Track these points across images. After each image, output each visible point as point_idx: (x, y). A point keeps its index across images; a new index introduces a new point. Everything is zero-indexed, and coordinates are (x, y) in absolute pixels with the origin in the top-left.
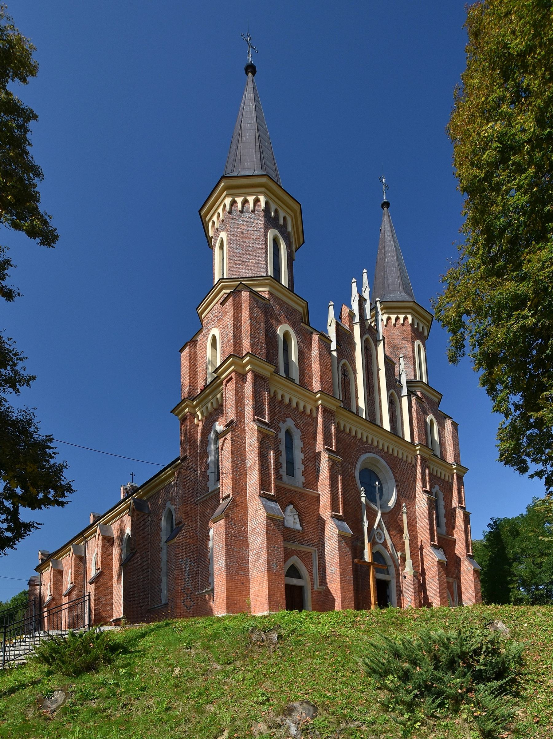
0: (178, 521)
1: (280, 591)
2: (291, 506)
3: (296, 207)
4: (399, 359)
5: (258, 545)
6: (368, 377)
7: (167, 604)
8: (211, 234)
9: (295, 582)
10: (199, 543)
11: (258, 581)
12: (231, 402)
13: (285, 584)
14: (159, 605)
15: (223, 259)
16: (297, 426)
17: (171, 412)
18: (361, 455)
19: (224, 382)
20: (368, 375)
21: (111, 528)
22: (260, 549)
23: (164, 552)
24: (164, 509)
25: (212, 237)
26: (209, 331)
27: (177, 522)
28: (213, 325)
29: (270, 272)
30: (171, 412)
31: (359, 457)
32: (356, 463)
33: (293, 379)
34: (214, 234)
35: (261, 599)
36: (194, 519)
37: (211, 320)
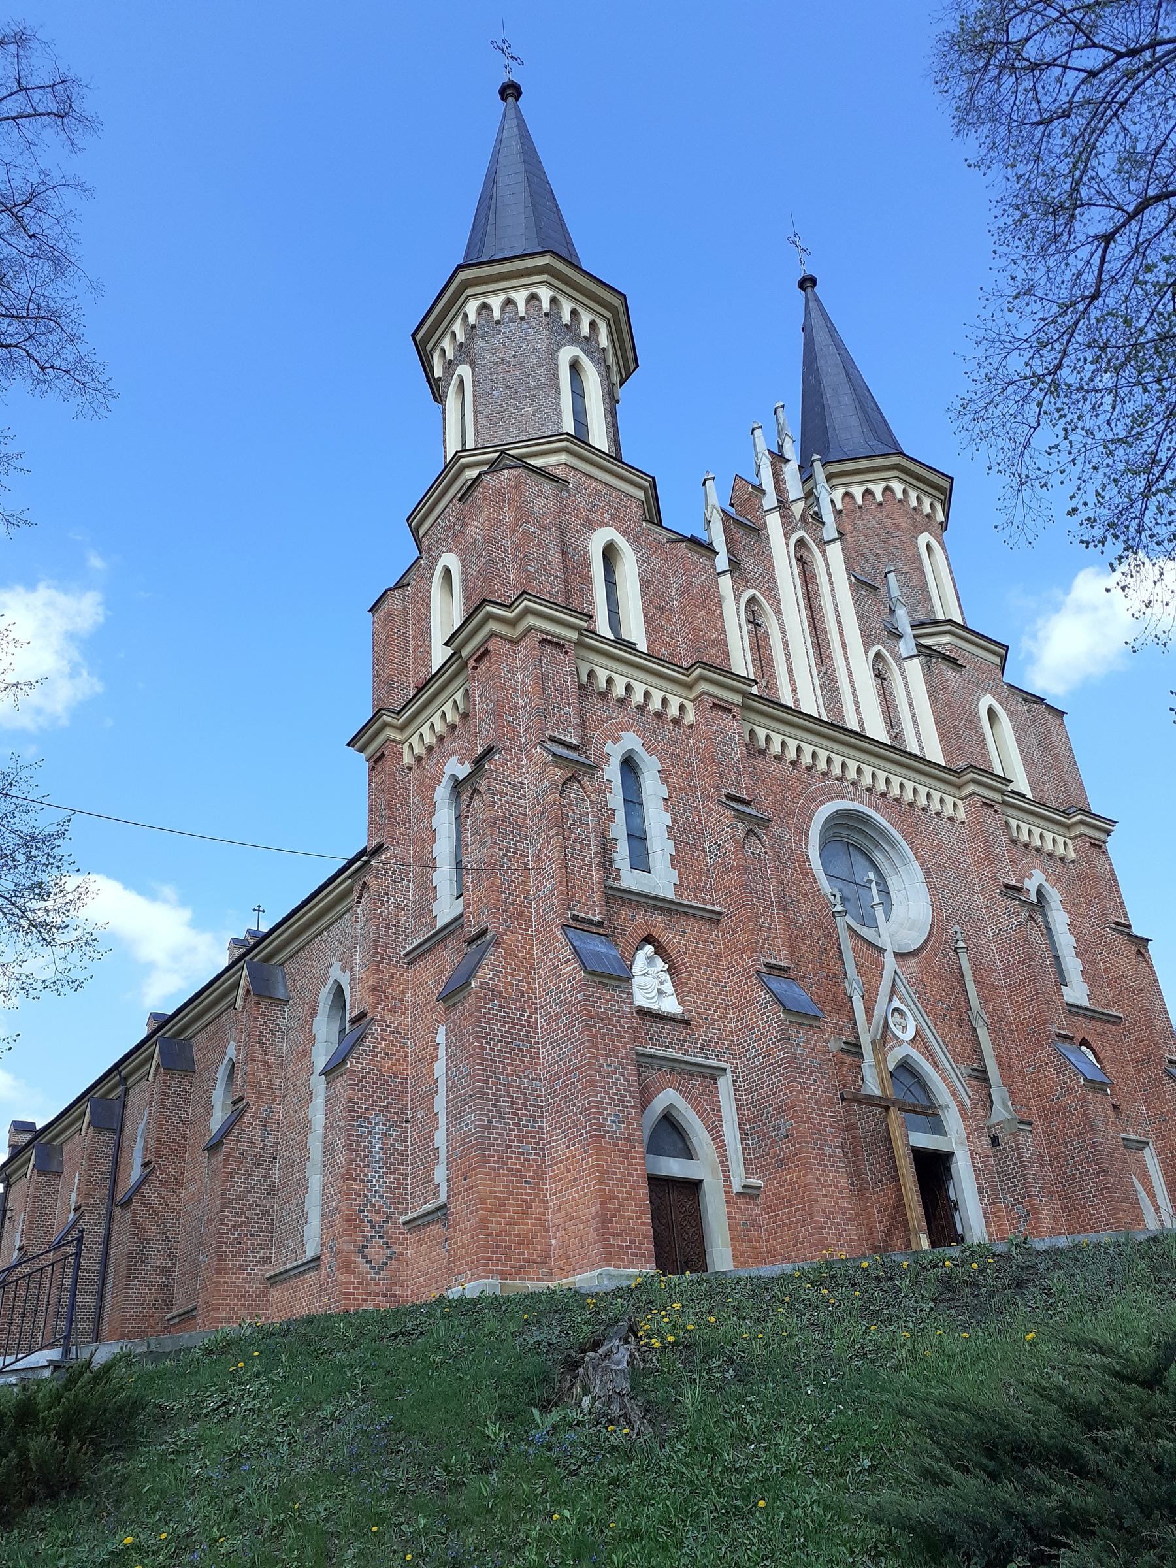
0: (356, 1012)
1: (633, 1199)
2: (649, 949)
3: (615, 301)
4: (886, 576)
5: (565, 1063)
6: (814, 624)
7: (317, 1259)
8: (438, 372)
9: (674, 1167)
10: (411, 1071)
11: (568, 1170)
12: (488, 705)
13: (649, 1178)
14: (299, 1262)
15: (463, 416)
16: (648, 748)
17: (348, 745)
18: (818, 807)
19: (471, 663)
20: (813, 619)
21: (191, 1046)
22: (571, 1072)
23: (319, 1102)
24: (324, 983)
25: (440, 379)
26: (434, 561)
27: (353, 1015)
28: (443, 546)
29: (569, 426)
30: (348, 745)
31: (813, 813)
32: (809, 827)
33: (631, 643)
34: (444, 373)
35: (582, 1226)
36: (399, 1003)
37: (440, 539)
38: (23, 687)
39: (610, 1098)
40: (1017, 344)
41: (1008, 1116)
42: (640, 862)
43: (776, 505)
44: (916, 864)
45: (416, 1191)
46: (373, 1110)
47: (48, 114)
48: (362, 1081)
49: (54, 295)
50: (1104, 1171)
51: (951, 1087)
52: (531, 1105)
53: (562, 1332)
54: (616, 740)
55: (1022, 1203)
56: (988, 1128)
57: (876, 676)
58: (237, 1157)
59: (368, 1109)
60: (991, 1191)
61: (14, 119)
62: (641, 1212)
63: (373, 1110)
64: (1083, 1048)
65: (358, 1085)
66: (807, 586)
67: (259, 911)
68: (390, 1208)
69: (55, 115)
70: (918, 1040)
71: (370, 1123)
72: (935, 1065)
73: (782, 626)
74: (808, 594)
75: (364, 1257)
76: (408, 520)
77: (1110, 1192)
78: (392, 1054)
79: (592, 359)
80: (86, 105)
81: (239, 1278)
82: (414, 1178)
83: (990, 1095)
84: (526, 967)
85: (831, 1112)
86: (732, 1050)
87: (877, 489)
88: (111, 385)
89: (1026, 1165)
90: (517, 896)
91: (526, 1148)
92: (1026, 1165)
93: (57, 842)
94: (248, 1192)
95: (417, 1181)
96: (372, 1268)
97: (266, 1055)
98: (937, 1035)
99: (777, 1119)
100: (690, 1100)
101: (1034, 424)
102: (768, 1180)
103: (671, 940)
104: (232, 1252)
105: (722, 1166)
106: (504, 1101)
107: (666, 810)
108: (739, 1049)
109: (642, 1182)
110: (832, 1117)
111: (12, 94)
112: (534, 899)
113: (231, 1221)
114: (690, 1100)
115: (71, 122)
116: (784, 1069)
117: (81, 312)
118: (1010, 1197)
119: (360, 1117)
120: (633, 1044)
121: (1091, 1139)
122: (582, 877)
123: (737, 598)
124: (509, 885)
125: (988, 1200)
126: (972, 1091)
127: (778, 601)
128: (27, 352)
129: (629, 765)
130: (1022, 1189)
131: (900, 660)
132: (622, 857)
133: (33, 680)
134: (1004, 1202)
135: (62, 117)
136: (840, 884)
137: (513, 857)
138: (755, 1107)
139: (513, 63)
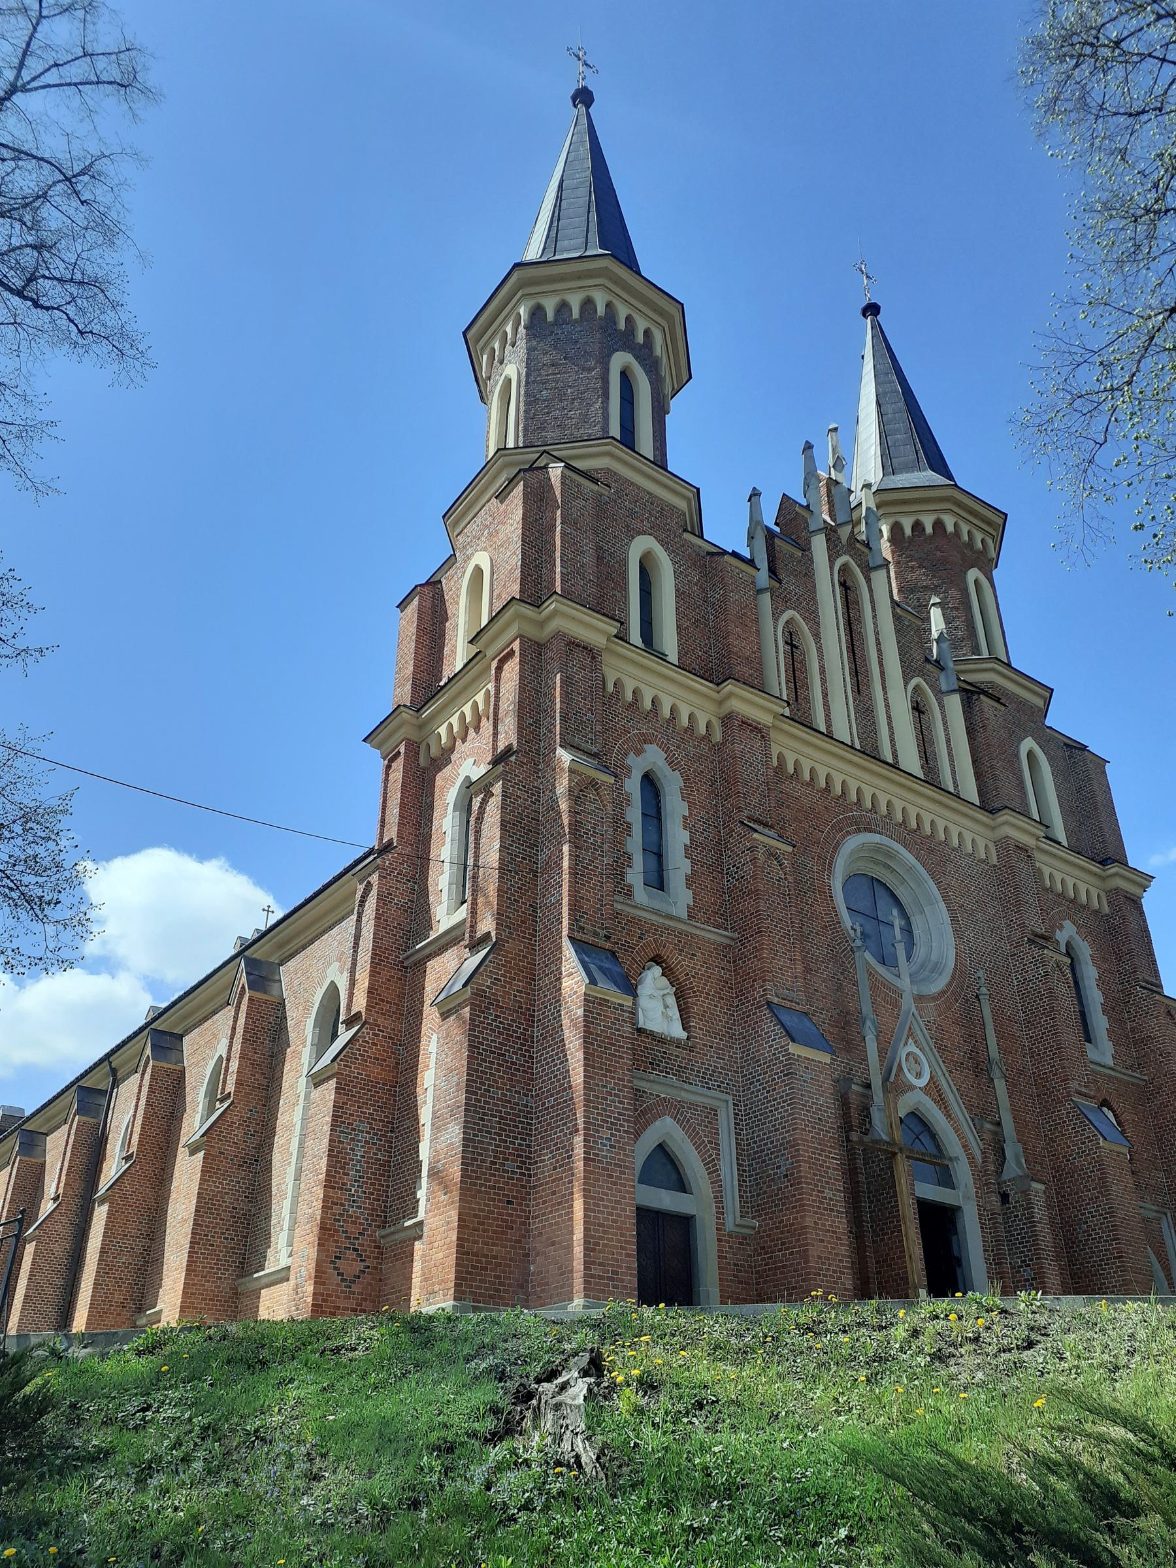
9: (666, 1200)
17: (364, 740)
30: (364, 740)
38: (33, 652)
39: (602, 1121)
40: (1087, 357)
41: (1020, 1173)
42: (658, 881)
43: (823, 526)
44: (943, 905)
45: (396, 1205)
46: (357, 1116)
47: (111, 83)
48: (349, 1086)
49: (99, 261)
50: (1118, 1239)
51: (963, 1138)
52: (520, 1122)
53: (519, 1358)
54: (639, 752)
55: (1029, 1265)
56: (998, 1184)
57: (913, 708)
58: (217, 1156)
59: (353, 1115)
60: (997, 1250)
61: (75, 85)
62: (626, 1242)
63: (357, 1116)
64: (1105, 1109)
65: (344, 1089)
66: (848, 612)
67: (268, 911)
68: (367, 1220)
69: (119, 84)
70: (933, 1090)
71: (354, 1130)
72: (948, 1116)
73: (820, 650)
74: (849, 620)
75: (335, 1268)
76: (444, 517)
77: (1123, 1262)
78: (382, 1060)
79: (643, 366)
80: (151, 77)
81: (209, 1281)
82: (395, 1190)
83: (1003, 1149)
84: (527, 978)
85: (835, 1154)
86: (736, 1081)
88: (149, 354)
89: (1035, 1226)
90: (523, 903)
91: (511, 1166)
92: (1035, 1226)
93: (59, 817)
94: (226, 1193)
95: (397, 1194)
96: (343, 1280)
97: (255, 1053)
98: (952, 1083)
99: (777, 1157)
100: (688, 1130)
101: (1101, 439)
102: (763, 1220)
103: (680, 962)
104: (204, 1254)
105: (716, 1202)
106: (492, 1115)
107: (685, 828)
108: (743, 1082)
109: (631, 1212)
110: (835, 1159)
111: (77, 59)
112: (541, 907)
113: (205, 1221)
114: (688, 1130)
115: (133, 93)
116: (788, 1105)
117: (126, 279)
118: (1018, 1258)
119: (344, 1123)
120: (631, 1066)
121: (1106, 1204)
122: (591, 888)
123: (776, 618)
124: (515, 891)
125: (994, 1260)
126: (984, 1144)
127: (818, 623)
128: (67, 315)
129: (649, 780)
130: (1031, 1251)
131: (940, 694)
132: (635, 876)
133: (44, 646)
134: (1010, 1263)
135: (125, 87)
136: (860, 919)
137: (522, 863)
138: (755, 1142)
139: (588, 72)
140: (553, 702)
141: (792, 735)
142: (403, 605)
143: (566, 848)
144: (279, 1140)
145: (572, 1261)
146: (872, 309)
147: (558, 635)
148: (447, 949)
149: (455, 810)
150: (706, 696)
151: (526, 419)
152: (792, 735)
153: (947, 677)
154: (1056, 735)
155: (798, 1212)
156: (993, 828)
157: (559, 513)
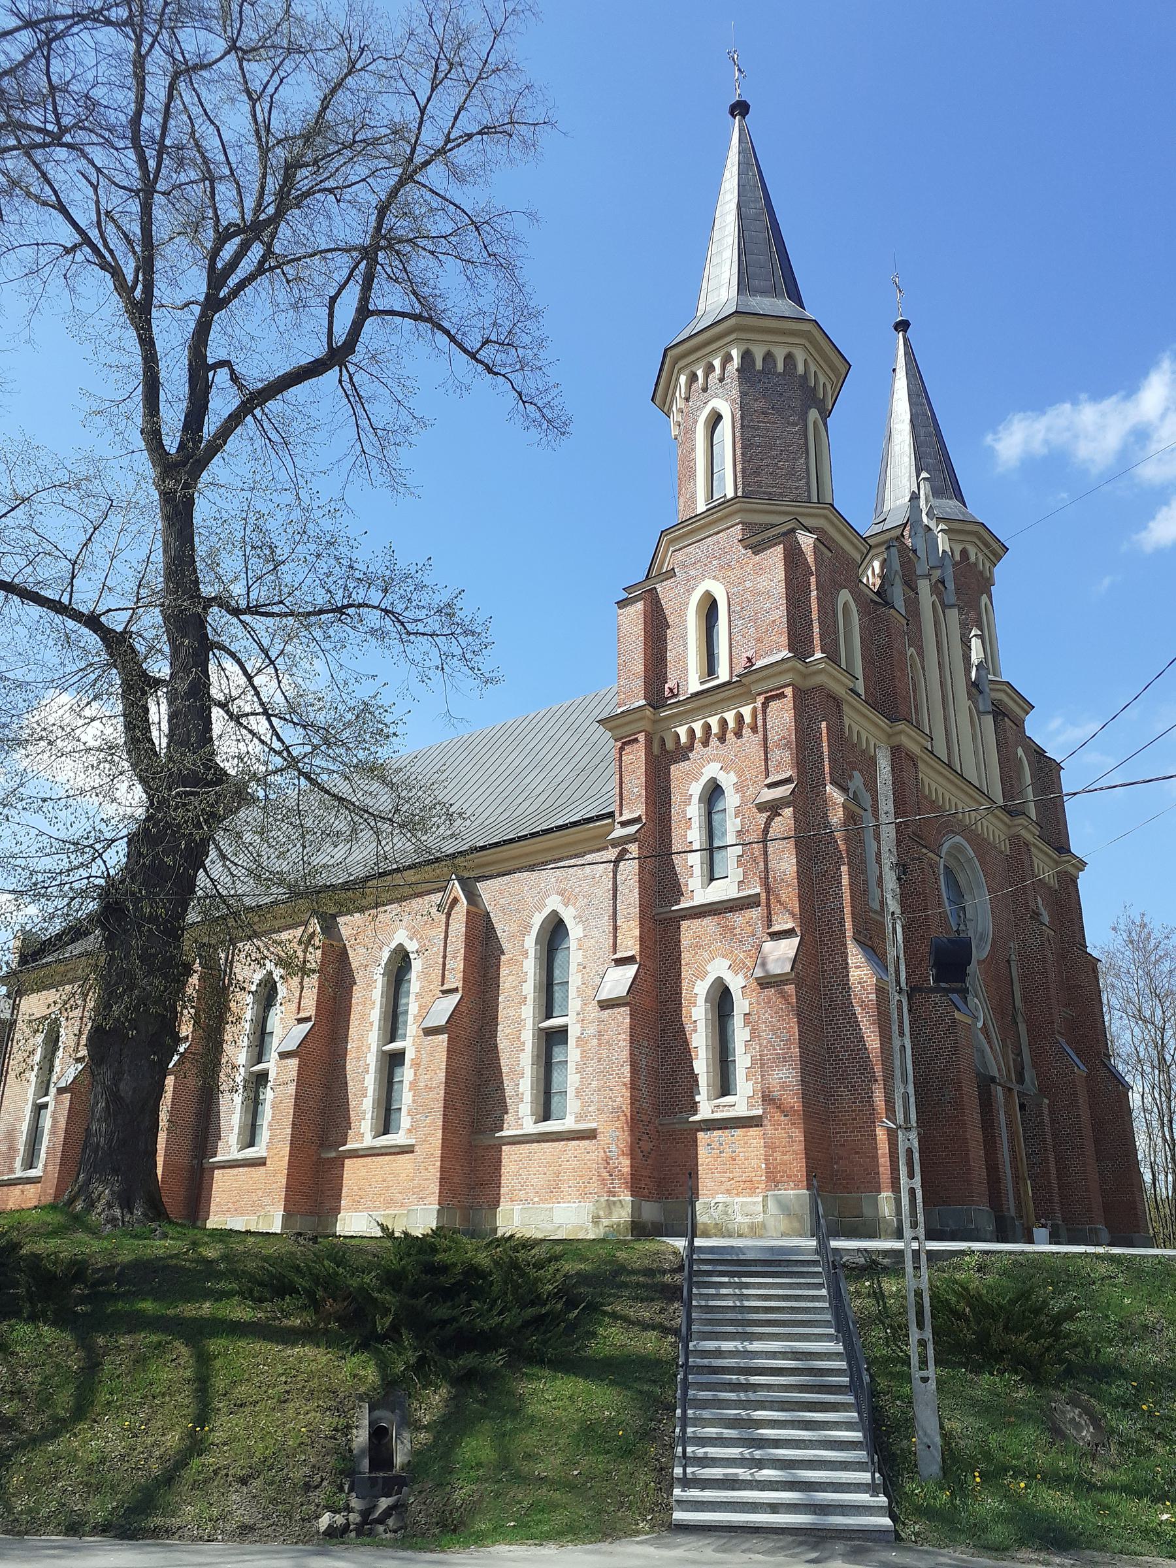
72: (991, 1048)
87: (780, 354)
140: (820, 744)
141: (932, 768)
142: (623, 603)
143: (844, 869)
144: (357, 994)
145: (878, 1167)
146: (902, 326)
147: (820, 688)
148: (705, 916)
149: (700, 801)
150: (882, 729)
151: (744, 461)
152: (932, 768)
153: (984, 699)
154: (1032, 744)
155: (960, 1128)
156: (1009, 827)
157: (813, 579)
